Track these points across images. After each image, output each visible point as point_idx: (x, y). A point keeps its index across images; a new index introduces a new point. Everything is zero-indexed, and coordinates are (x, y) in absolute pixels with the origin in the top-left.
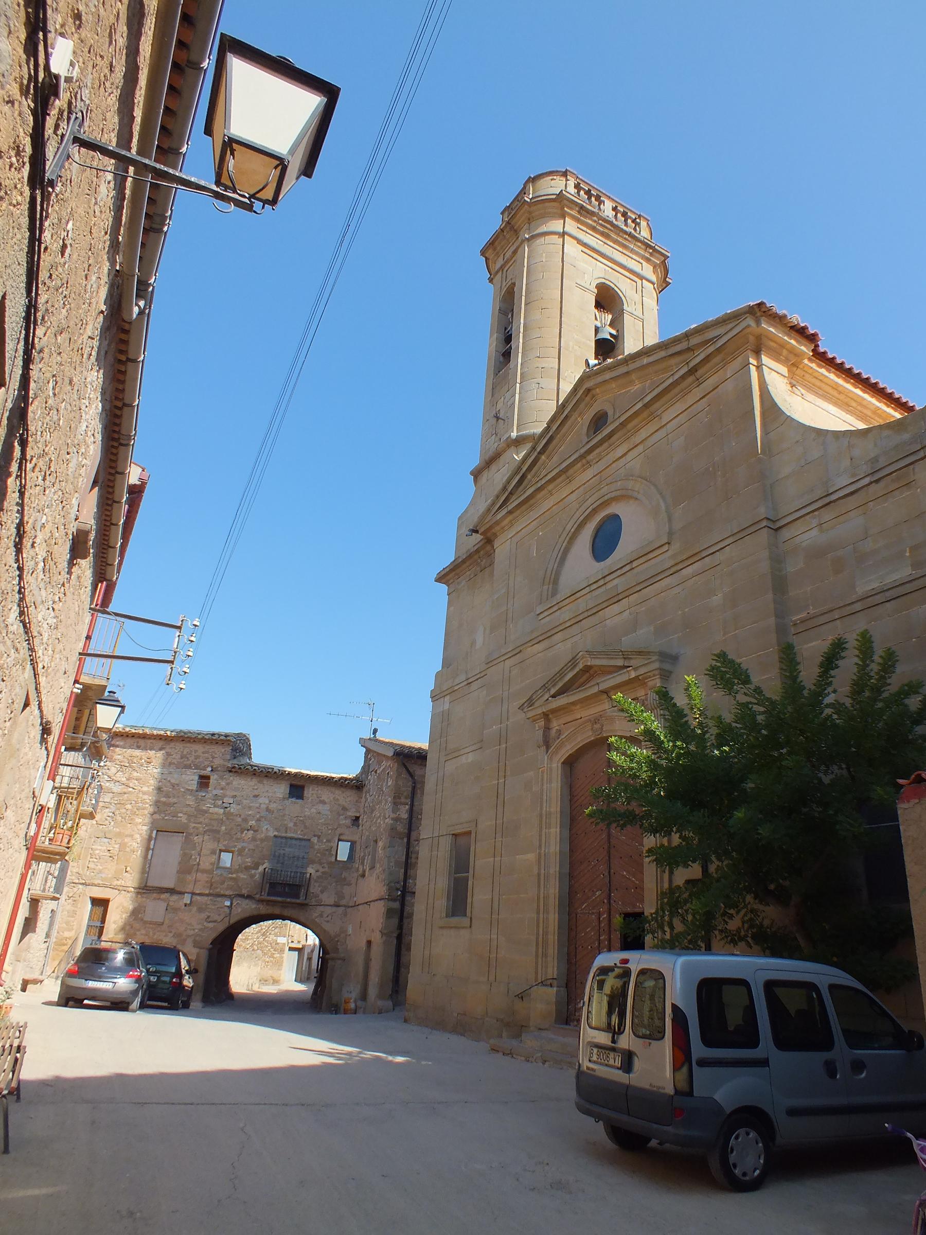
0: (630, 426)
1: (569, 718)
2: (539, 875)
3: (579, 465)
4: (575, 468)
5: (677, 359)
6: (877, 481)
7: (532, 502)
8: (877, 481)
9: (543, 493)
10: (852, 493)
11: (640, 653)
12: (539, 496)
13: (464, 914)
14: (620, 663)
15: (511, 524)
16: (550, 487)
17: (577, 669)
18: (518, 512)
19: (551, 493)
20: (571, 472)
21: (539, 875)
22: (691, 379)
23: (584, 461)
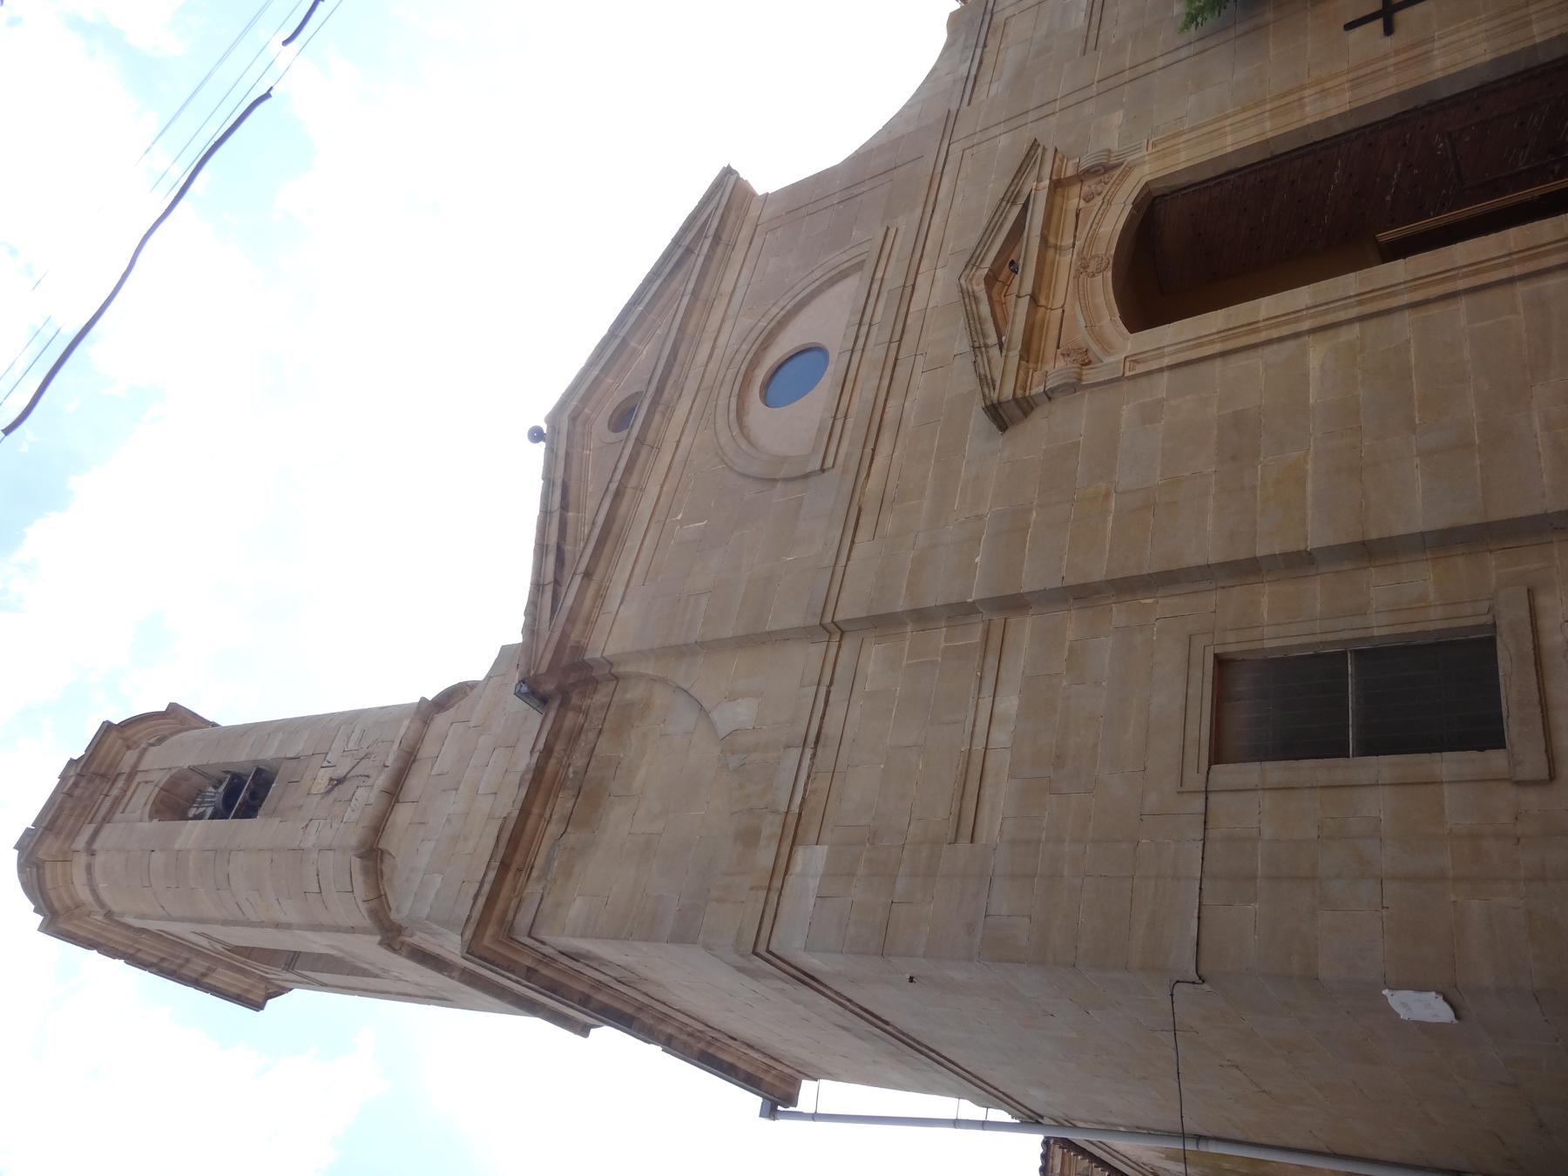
0: (690, 329)
1: (1054, 332)
2: (1361, 318)
3: (658, 417)
4: (654, 425)
5: (679, 277)
6: (985, 46)
7: (615, 529)
8: (985, 46)
9: (626, 500)
10: (981, 63)
11: (1021, 171)
12: (622, 510)
13: (1504, 747)
14: (1016, 210)
15: (601, 596)
16: (633, 481)
17: (983, 296)
18: (602, 564)
19: (640, 489)
20: (651, 436)
21: (1361, 318)
22: (720, 249)
23: (660, 408)
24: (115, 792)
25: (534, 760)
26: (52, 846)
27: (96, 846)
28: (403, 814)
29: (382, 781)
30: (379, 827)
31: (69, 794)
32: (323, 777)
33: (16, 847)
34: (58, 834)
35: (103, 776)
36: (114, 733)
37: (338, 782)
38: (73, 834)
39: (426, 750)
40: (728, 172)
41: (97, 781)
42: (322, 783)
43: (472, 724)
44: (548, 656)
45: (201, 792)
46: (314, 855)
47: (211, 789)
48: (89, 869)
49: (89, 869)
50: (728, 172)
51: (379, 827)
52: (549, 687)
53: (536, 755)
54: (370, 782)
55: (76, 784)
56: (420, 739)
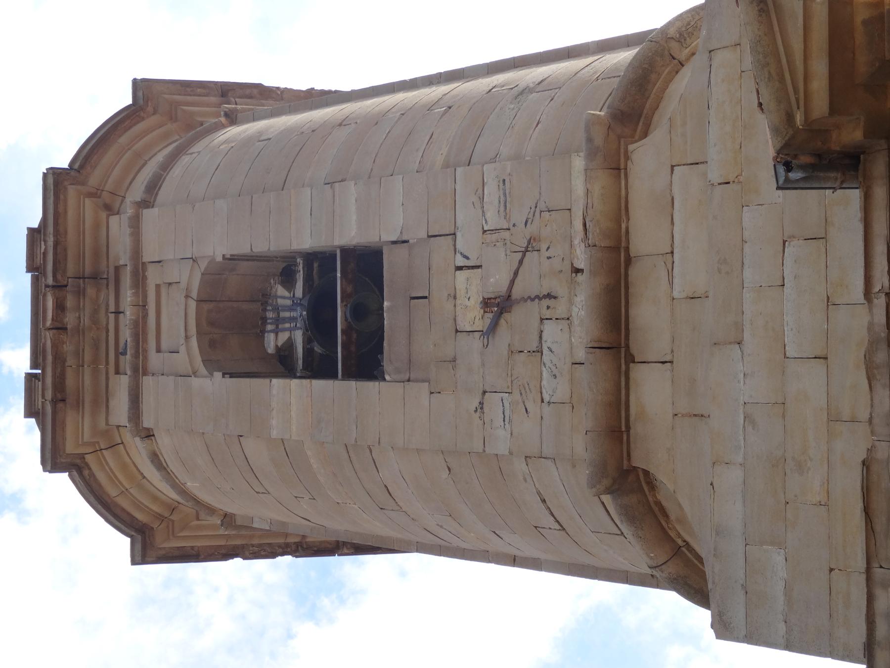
24: (129, 314)
25: (880, 317)
26: (79, 431)
27: (147, 422)
28: (652, 391)
29: (581, 304)
30: (617, 426)
31: (60, 328)
32: (470, 291)
33: (137, 84)
34: (79, 404)
35: (95, 277)
36: (72, 191)
37: (499, 306)
38: (102, 400)
39: (645, 237)
40: (134, 562)
41: (90, 291)
42: (472, 316)
43: (715, 176)
44: (820, 68)
45: (265, 298)
46: (520, 466)
47: (281, 291)
48: (155, 458)
49: (155, 458)
50: (134, 562)
51: (617, 426)
52: (852, 134)
53: (880, 302)
54: (561, 309)
55: (60, 307)
56: (620, 210)
